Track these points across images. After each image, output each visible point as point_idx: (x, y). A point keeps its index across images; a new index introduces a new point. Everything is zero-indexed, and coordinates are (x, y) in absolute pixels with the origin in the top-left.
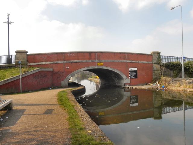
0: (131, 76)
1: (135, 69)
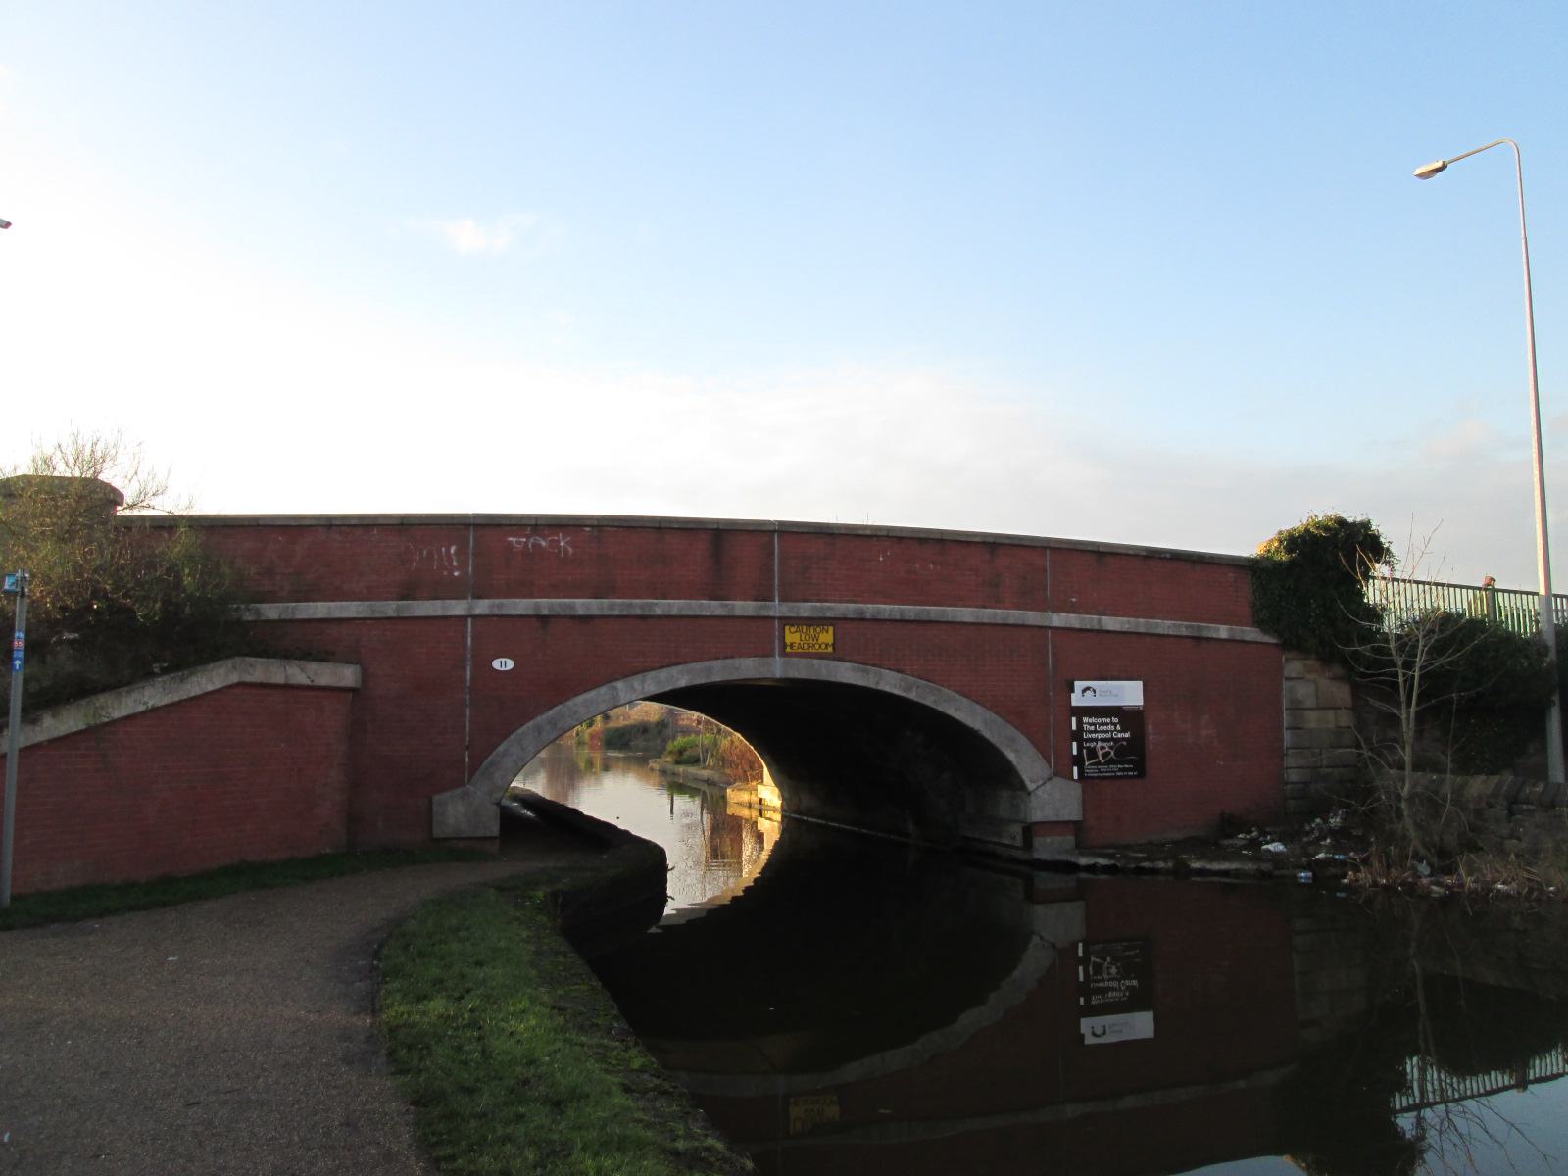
0: (1092, 753)
1: (1130, 693)
